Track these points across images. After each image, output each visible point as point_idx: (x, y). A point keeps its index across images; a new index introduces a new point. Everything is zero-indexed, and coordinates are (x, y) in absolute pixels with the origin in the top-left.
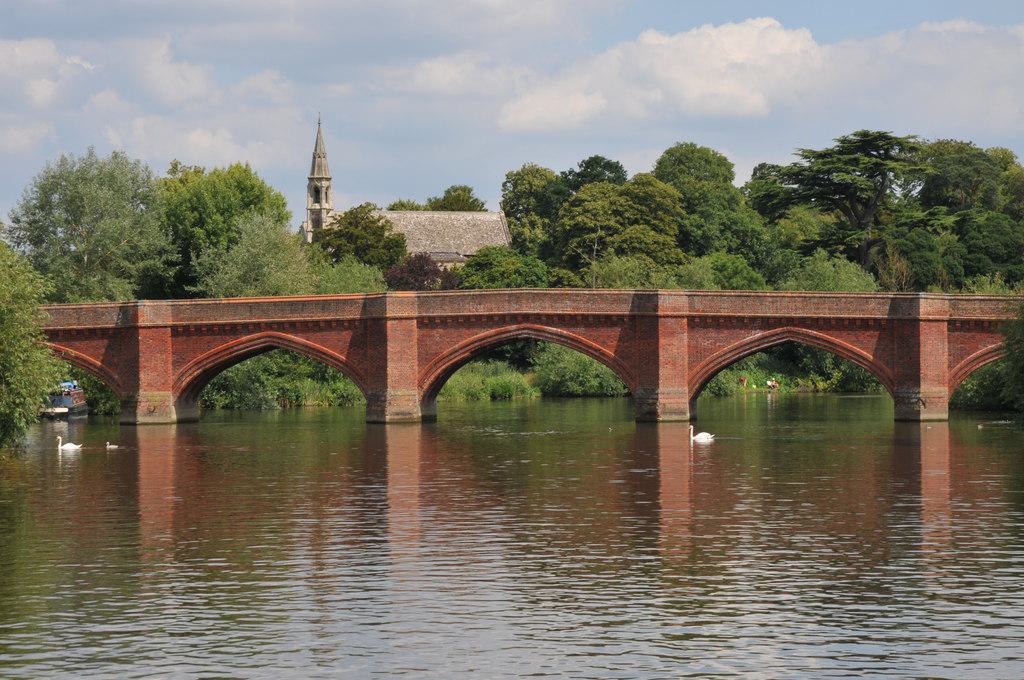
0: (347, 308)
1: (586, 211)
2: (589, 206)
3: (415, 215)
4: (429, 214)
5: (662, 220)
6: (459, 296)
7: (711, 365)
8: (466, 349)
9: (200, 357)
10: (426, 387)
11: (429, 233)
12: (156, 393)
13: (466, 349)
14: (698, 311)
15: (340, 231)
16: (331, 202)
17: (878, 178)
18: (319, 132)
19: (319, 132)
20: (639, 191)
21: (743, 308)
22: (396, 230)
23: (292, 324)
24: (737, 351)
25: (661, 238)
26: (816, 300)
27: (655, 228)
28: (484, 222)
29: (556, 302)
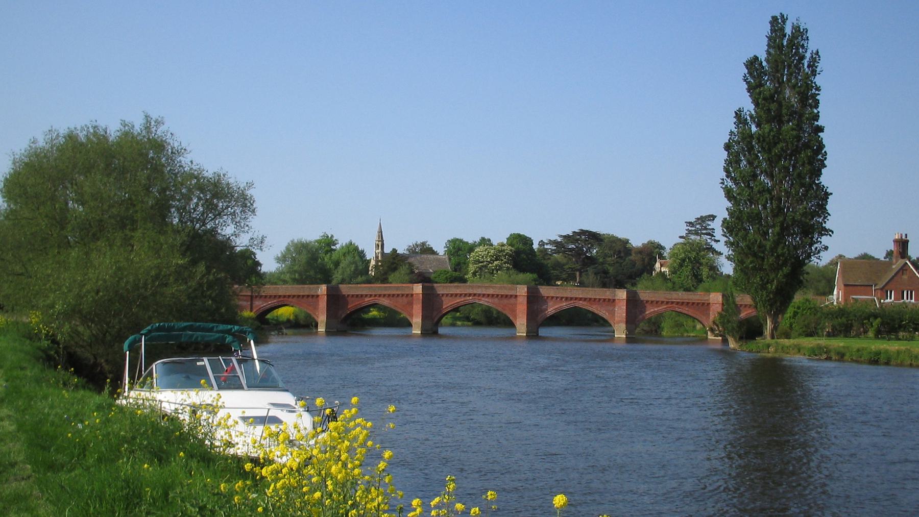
18: (381, 232)
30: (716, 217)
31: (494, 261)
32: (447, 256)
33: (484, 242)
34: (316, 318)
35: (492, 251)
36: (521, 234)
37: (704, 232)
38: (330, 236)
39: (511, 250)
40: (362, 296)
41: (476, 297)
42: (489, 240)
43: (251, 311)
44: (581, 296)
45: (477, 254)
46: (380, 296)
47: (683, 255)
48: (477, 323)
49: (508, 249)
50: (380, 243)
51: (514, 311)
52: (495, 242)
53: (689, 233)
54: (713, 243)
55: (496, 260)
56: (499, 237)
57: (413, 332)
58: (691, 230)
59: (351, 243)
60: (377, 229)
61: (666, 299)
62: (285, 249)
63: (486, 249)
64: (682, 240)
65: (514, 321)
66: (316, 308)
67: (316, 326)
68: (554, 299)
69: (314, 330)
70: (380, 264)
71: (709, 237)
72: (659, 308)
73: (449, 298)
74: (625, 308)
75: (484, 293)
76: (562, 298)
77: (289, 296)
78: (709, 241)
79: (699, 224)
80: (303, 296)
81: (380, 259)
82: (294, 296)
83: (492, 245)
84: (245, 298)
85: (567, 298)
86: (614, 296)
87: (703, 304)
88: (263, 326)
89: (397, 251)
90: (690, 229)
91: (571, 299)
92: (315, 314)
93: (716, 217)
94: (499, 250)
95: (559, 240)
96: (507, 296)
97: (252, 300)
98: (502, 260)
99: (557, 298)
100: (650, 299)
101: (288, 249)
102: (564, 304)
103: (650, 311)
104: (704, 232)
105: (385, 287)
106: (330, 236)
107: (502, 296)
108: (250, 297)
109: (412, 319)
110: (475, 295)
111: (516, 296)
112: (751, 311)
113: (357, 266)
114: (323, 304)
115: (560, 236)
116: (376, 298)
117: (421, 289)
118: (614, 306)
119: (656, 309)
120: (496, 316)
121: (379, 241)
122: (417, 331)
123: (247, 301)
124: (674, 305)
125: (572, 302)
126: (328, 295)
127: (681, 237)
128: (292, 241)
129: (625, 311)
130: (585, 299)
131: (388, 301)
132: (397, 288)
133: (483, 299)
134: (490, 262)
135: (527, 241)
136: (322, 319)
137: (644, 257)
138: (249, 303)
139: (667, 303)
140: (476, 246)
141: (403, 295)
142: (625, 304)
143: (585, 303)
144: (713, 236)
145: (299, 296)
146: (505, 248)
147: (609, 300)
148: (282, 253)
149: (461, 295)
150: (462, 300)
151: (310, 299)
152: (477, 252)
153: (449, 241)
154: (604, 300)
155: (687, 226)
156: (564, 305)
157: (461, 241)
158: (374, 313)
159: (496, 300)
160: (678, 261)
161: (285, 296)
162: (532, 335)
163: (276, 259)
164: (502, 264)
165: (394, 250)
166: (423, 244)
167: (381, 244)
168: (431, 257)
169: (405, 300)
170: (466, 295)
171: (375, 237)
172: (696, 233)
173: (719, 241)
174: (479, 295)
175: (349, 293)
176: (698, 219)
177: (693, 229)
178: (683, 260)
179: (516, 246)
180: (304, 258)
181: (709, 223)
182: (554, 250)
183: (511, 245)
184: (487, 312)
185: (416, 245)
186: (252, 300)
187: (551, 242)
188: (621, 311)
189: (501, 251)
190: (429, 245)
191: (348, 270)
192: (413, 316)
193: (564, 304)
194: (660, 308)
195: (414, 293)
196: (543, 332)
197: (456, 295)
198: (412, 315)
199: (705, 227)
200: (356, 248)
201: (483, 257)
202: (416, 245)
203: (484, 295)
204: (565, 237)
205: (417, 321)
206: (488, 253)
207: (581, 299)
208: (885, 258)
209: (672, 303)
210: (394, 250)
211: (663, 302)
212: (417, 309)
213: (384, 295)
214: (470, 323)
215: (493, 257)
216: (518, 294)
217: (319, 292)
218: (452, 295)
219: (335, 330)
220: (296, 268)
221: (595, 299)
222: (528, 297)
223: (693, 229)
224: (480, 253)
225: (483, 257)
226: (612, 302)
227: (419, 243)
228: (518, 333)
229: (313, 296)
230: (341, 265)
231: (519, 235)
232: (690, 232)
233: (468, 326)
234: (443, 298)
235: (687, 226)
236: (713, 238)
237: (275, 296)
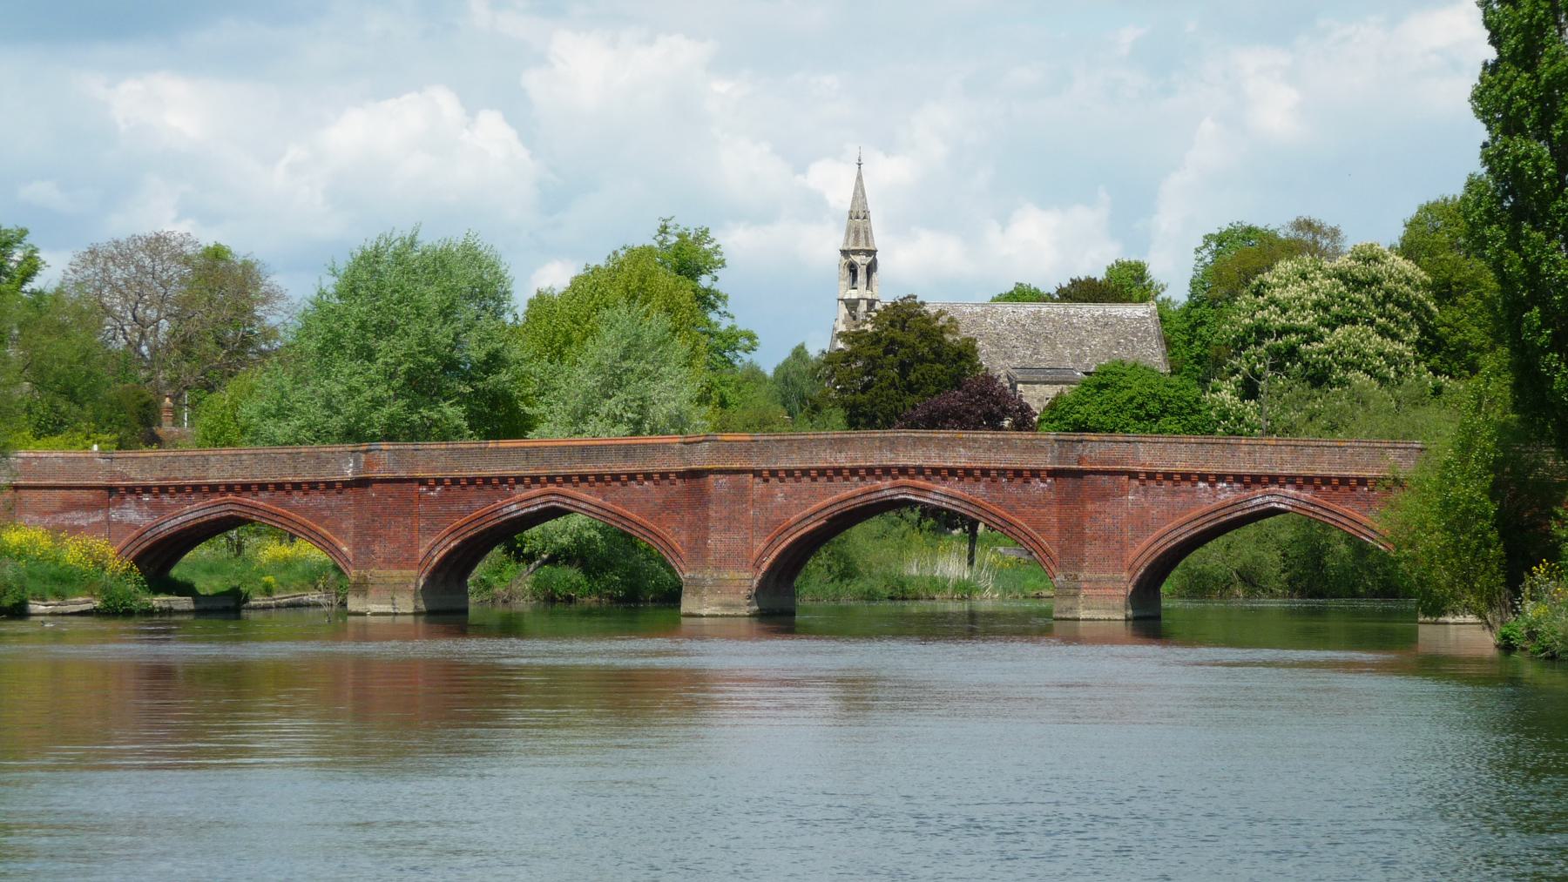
0: (659, 455)
1: (1273, 301)
2: (1278, 293)
3: (1010, 309)
4: (1059, 308)
5: (1391, 317)
6: (944, 439)
7: (1162, 542)
8: (819, 515)
9: (459, 522)
10: (764, 567)
11: (1032, 339)
12: (396, 573)
13: (819, 515)
14: (1143, 465)
15: (876, 334)
16: (875, 288)
17: (1379, 294)
18: (859, 178)
19: (859, 178)
20: (1359, 270)
21: (1207, 461)
22: (964, 333)
23: (583, 478)
24: (1199, 522)
25: (1390, 346)
26: (1310, 451)
27: (1384, 332)
28: (1121, 319)
29: (945, 449)
145: (279, 486)
149: (854, 471)
170: (870, 471)
175: (456, 474)
197: (838, 471)
218: (822, 472)
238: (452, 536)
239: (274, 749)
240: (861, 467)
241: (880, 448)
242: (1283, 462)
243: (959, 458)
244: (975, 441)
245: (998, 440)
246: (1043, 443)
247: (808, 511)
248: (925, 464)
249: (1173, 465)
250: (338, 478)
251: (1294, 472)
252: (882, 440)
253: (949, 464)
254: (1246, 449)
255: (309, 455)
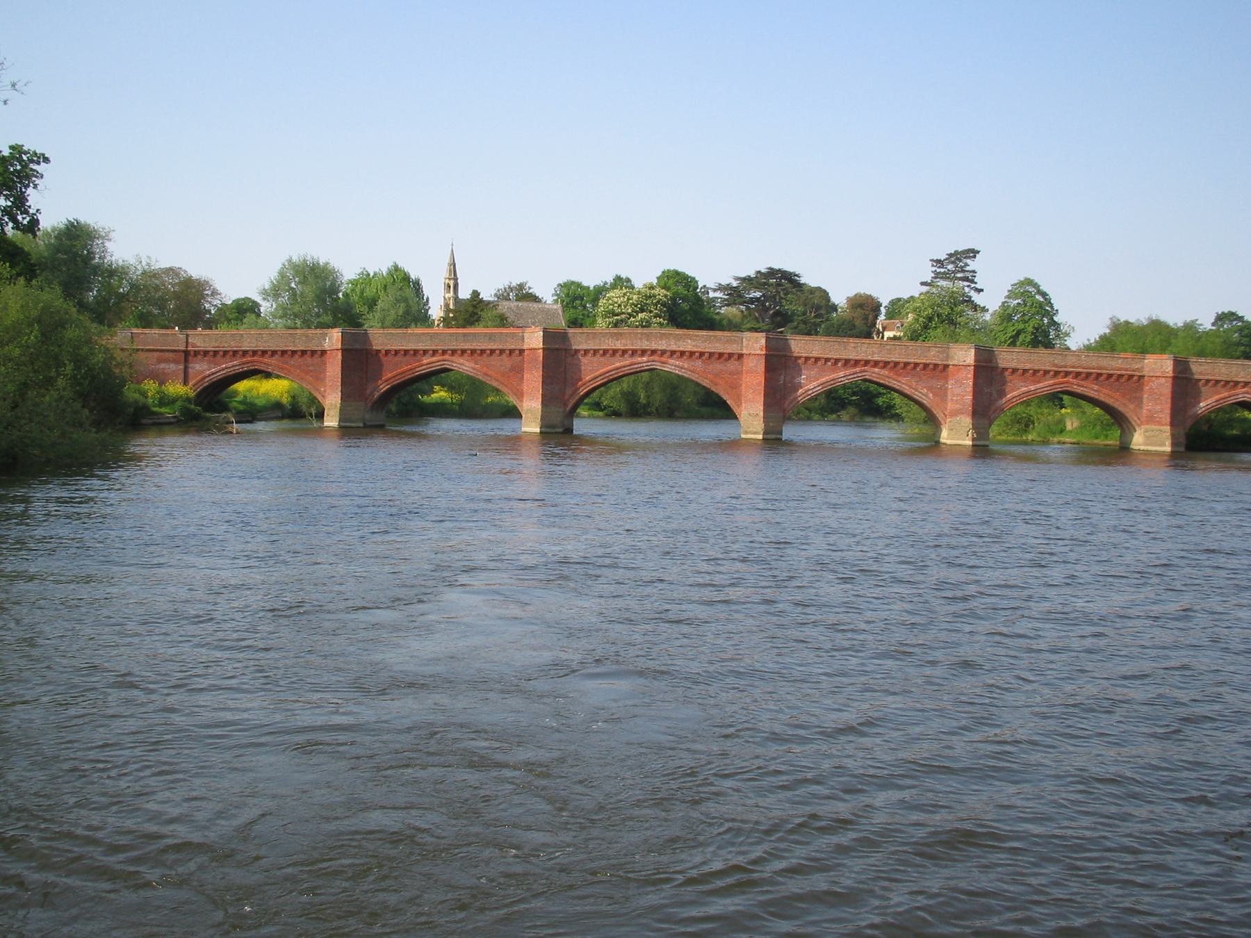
6: (679, 334)
18: (452, 251)
19: (452, 251)
26: (889, 347)
30: (978, 252)
31: (637, 313)
32: (559, 305)
33: (620, 282)
34: (320, 398)
35: (635, 297)
36: (680, 270)
37: (959, 275)
38: (372, 275)
39: (666, 296)
40: (416, 352)
41: (656, 358)
42: (628, 280)
43: (185, 383)
44: (876, 358)
45: (610, 302)
46: (454, 352)
47: (930, 311)
48: (616, 414)
49: (660, 293)
50: (452, 283)
51: (735, 387)
52: (639, 284)
53: (936, 278)
54: (973, 294)
55: (642, 311)
56: (644, 276)
57: (524, 429)
58: (940, 272)
59: (396, 268)
60: (447, 260)
61: (1056, 366)
62: (276, 274)
63: (625, 294)
64: (925, 289)
65: (735, 409)
66: (319, 376)
67: (320, 415)
68: (819, 363)
69: (316, 424)
70: (451, 315)
71: (966, 283)
72: (1038, 386)
73: (598, 358)
74: (971, 383)
75: (674, 348)
76: (837, 361)
77: (264, 352)
78: (967, 290)
79: (953, 262)
80: (294, 352)
81: (451, 307)
82: (274, 353)
83: (633, 288)
84: (171, 355)
85: (847, 362)
86: (947, 358)
87: (1131, 377)
88: (208, 415)
89: (479, 294)
90: (938, 270)
91: (857, 362)
92: (318, 390)
93: (978, 252)
94: (646, 296)
95: (735, 284)
96: (721, 355)
97: (186, 361)
98: (651, 312)
99: (827, 360)
100: (1021, 366)
101: (282, 274)
102: (842, 374)
103: (1017, 390)
104: (959, 275)
105: (465, 335)
106: (372, 275)
107: (711, 354)
108: (183, 354)
109: (522, 401)
110: (654, 352)
111: (740, 356)
112: (1226, 394)
113: (408, 306)
114: (334, 369)
115: (737, 279)
116: (446, 357)
117: (541, 339)
118: (946, 379)
119: (1032, 388)
120: (644, 402)
121: (450, 279)
122: (531, 426)
123: (176, 362)
124: (1069, 379)
125: (858, 369)
126: (344, 351)
127: (923, 284)
128: (290, 261)
129: (970, 389)
130: (886, 364)
131: (472, 365)
132: (491, 337)
133: (672, 361)
134: (630, 315)
135: (686, 282)
136: (332, 401)
137: (867, 313)
138: (181, 367)
139: (1056, 373)
140: (607, 290)
141: (502, 351)
142: (971, 375)
143: (885, 372)
144: (972, 281)
145: (284, 352)
146: (657, 291)
147: (936, 365)
148: (272, 282)
149: (624, 352)
150: (627, 362)
151: (308, 359)
152: (609, 298)
153: (559, 285)
154: (926, 366)
155: (933, 266)
156: (842, 376)
157: (579, 285)
158: (440, 394)
159: (699, 363)
160: (921, 319)
161: (255, 353)
162: (773, 442)
163: (49, 161)
164: (650, 318)
165: (476, 294)
166: (521, 286)
167: (453, 284)
168: (535, 305)
169: (506, 362)
170: (634, 352)
171: (444, 272)
172: (945, 276)
173: (982, 290)
174: (663, 352)
175: (388, 348)
176: (951, 255)
177: (942, 270)
178: (930, 319)
179: (674, 289)
180: (310, 291)
181: (968, 261)
182: (725, 300)
183: (665, 287)
184: (674, 385)
185: (509, 287)
186: (186, 361)
187: (721, 288)
188: (961, 390)
189: (650, 297)
190: (530, 288)
191: (393, 312)
192: (522, 395)
193: (842, 374)
194: (1041, 385)
195: (525, 347)
196: (790, 432)
197: (615, 352)
198: (520, 395)
199: (962, 267)
200: (406, 278)
201: (620, 306)
202: (509, 287)
203: (673, 353)
204: (744, 280)
205: (532, 406)
206: (628, 299)
207: (876, 364)
208: (1213, 324)
209: (1067, 374)
210: (476, 294)
211: (1046, 372)
212: (533, 380)
213: (463, 352)
214: (601, 414)
215: (636, 306)
216: (744, 351)
217: (327, 345)
218: (605, 352)
219: (361, 425)
220: (297, 309)
221: (906, 364)
222: (768, 358)
223: (942, 270)
224: (616, 300)
225: (620, 306)
226: (941, 370)
227: (514, 284)
228: (746, 433)
229: (313, 352)
230: (380, 304)
231: (677, 273)
232: (937, 275)
233: (598, 417)
234: (584, 360)
235: (933, 266)
236: (973, 285)
237: (235, 353)
238: (386, 383)
239: (1151, 783)
240: (629, 350)
241: (641, 339)
242: (873, 353)
243: (688, 346)
244: (697, 336)
245: (711, 336)
246: (736, 339)
247: (598, 373)
248: (667, 349)
249: (811, 353)
250: (320, 348)
251: (879, 359)
252: (642, 334)
253: (681, 349)
254: (852, 345)
255: (303, 335)
